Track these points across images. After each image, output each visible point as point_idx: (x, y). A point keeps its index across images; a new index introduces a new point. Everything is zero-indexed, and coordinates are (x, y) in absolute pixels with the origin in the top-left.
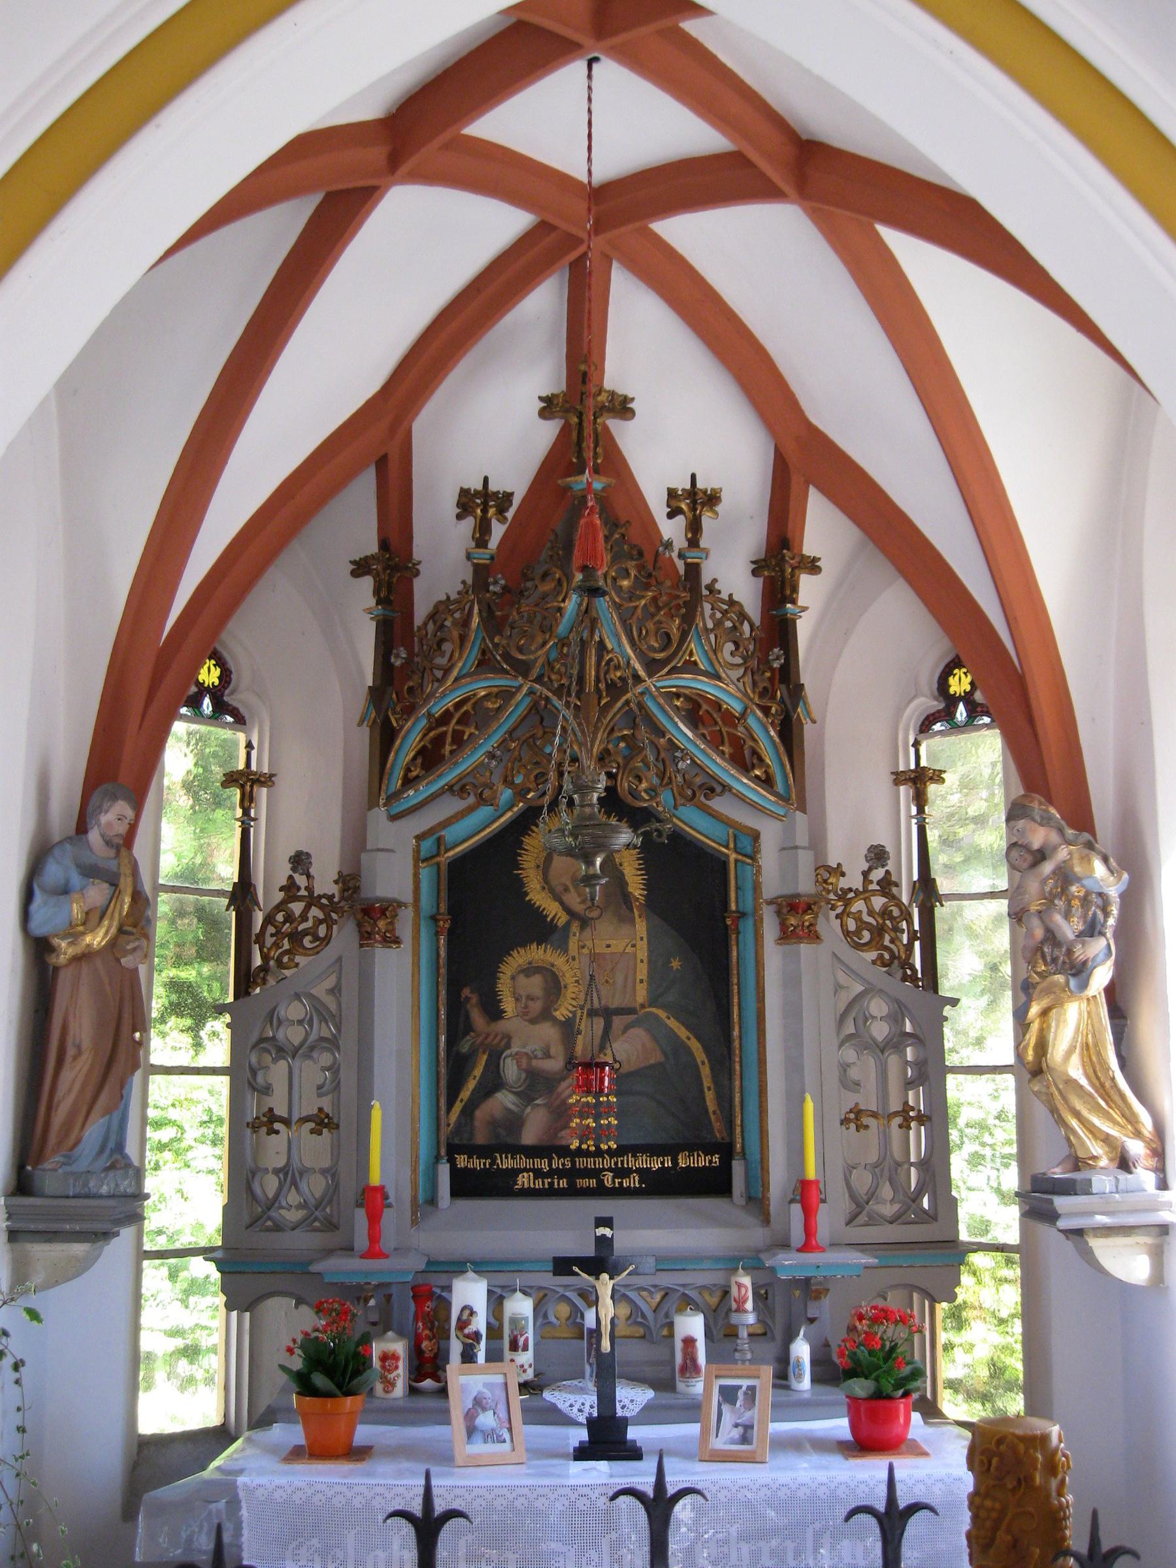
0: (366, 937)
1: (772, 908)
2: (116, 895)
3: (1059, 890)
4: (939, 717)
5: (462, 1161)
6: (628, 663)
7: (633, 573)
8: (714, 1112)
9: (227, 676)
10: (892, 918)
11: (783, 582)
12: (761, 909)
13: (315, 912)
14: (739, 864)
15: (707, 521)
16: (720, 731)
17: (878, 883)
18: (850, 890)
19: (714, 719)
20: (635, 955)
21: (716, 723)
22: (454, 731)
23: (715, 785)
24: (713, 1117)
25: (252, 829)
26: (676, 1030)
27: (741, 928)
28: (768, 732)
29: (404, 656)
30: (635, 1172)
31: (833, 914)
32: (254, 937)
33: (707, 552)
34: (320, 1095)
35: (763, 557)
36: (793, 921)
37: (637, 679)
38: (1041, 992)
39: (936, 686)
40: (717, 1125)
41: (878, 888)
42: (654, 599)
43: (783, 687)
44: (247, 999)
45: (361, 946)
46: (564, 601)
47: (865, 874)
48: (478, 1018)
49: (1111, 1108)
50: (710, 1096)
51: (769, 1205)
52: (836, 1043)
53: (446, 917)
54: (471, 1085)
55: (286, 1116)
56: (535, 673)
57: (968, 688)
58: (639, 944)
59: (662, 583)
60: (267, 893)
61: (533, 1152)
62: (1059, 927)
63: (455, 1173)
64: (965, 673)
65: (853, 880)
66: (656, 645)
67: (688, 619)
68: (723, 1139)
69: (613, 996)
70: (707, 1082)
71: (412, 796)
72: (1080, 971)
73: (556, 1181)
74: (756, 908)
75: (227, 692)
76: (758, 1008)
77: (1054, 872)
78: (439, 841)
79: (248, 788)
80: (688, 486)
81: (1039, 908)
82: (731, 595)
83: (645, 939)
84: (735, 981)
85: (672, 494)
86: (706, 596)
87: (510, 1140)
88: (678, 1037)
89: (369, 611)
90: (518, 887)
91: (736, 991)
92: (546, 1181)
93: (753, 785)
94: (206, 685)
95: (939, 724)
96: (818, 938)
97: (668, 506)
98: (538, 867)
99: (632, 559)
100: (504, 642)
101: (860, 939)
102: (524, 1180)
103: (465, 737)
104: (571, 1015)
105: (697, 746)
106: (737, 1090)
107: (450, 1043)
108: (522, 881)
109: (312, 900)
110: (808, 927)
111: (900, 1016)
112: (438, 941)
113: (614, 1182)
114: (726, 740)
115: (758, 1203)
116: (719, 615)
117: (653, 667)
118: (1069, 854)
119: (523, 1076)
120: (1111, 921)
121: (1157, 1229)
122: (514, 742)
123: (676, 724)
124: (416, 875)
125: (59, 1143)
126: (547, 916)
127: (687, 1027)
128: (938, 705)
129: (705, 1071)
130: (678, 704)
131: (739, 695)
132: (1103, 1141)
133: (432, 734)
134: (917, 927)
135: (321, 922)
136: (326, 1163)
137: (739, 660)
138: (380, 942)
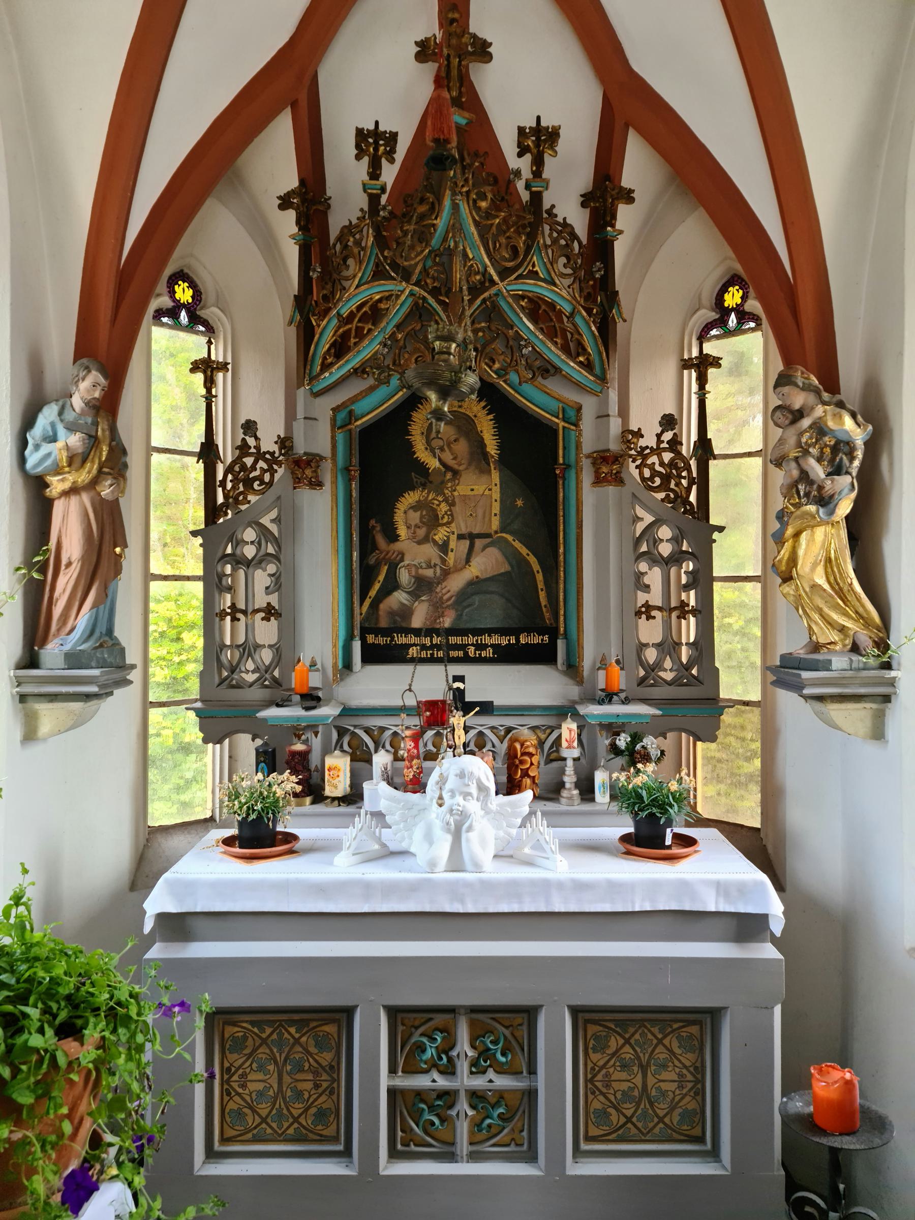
0: (297, 481)
1: (589, 461)
2: (96, 445)
3: (814, 440)
4: (716, 324)
5: (371, 639)
6: (486, 270)
7: (489, 196)
8: (545, 606)
9: (198, 296)
10: (677, 468)
11: (605, 211)
12: (582, 462)
13: (262, 464)
14: (565, 429)
15: (547, 158)
16: (554, 326)
17: (668, 443)
18: (647, 447)
19: (549, 316)
20: (491, 497)
21: (551, 320)
22: (357, 327)
23: (550, 367)
24: (544, 609)
25: (213, 404)
26: (519, 549)
27: (566, 476)
28: (590, 328)
29: (319, 270)
30: (490, 646)
31: (634, 465)
32: (218, 483)
33: (547, 182)
34: (267, 594)
35: (590, 189)
36: (605, 469)
37: (493, 283)
38: (795, 518)
39: (714, 301)
40: (547, 615)
41: (667, 446)
42: (505, 220)
43: (602, 293)
44: (214, 526)
45: (295, 488)
46: (436, 218)
47: (659, 436)
48: (381, 541)
49: (847, 606)
50: (542, 595)
51: (583, 671)
52: (633, 559)
53: (356, 468)
54: (377, 586)
55: (244, 608)
56: (414, 278)
57: (739, 301)
58: (494, 488)
59: (512, 206)
60: (227, 451)
61: (417, 632)
62: (813, 468)
63: (365, 647)
64: (738, 290)
65: (649, 441)
66: (507, 256)
67: (532, 237)
68: (551, 624)
69: (475, 526)
70: (541, 585)
71: (329, 378)
72: (825, 501)
73: (435, 652)
74: (578, 461)
75: (198, 307)
76: (577, 533)
77: (810, 427)
78: (351, 413)
79: (209, 373)
80: (534, 125)
81: (797, 454)
82: (565, 219)
83: (498, 485)
84: (561, 514)
85: (521, 130)
86: (546, 218)
87: (404, 625)
88: (520, 554)
89: (293, 237)
90: (409, 447)
91: (562, 521)
92: (428, 652)
93: (577, 368)
94: (182, 302)
95: (715, 330)
96: (622, 482)
97: (518, 147)
98: (423, 433)
99: (490, 185)
100: (391, 253)
101: (653, 483)
102: (413, 652)
103: (365, 332)
104: (446, 538)
105: (537, 337)
106: (561, 591)
107: (363, 556)
108: (412, 444)
109: (259, 455)
110: (615, 474)
111: (680, 538)
112: (351, 485)
113: (475, 653)
114: (559, 333)
115: (573, 669)
116: (555, 235)
117: (504, 273)
118: (824, 412)
119: (413, 580)
120: (856, 463)
121: (881, 698)
122: (400, 333)
123: (521, 319)
124: (333, 438)
125: (59, 630)
126: (429, 469)
127: (527, 547)
128: (714, 316)
129: (540, 577)
130: (523, 304)
131: (569, 298)
132: (840, 631)
133: (341, 331)
134: (695, 475)
135: (266, 471)
136: (274, 641)
137: (569, 271)
138: (307, 485)
